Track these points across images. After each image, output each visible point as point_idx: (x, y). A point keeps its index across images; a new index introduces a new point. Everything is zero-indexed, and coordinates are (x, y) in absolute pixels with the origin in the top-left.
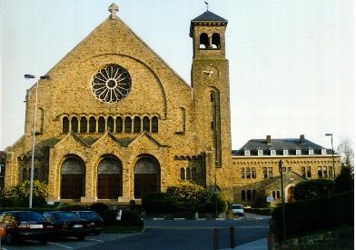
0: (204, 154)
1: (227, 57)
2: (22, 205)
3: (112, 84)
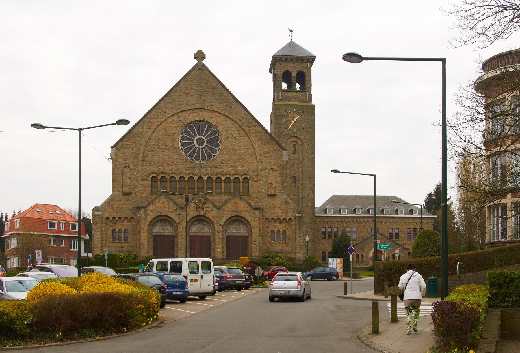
3: (200, 142)
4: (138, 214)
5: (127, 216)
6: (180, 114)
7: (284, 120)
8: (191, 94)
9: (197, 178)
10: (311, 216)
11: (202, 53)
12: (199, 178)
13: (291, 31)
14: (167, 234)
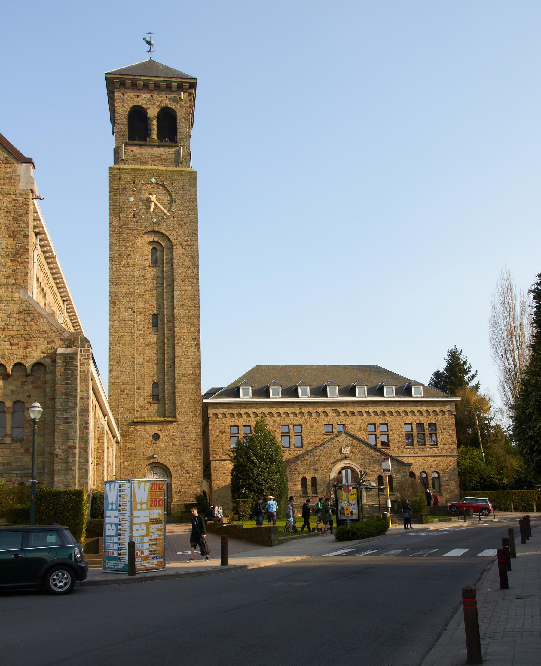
0: (53, 357)
7: (132, 199)
10: (193, 396)
13: (149, 43)
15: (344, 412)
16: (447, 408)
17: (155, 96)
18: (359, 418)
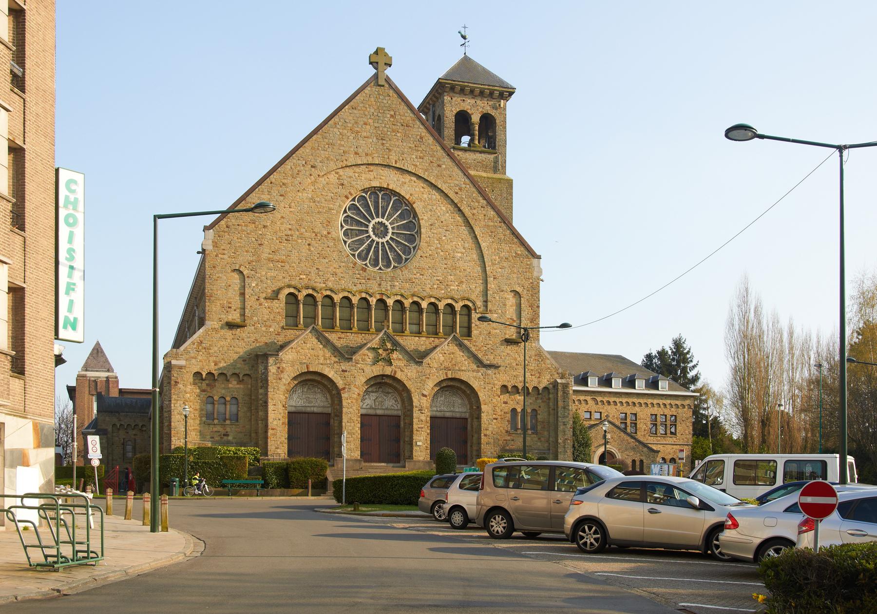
0: (555, 384)
1: (511, 172)
2: (764, 441)
4: (261, 368)
5: (237, 371)
6: (341, 172)
8: (364, 134)
9: (375, 300)
11: (386, 55)
12: (378, 300)
13: (464, 37)
14: (315, 410)
15: (602, 401)
16: (687, 402)
17: (478, 102)
18: (613, 406)
